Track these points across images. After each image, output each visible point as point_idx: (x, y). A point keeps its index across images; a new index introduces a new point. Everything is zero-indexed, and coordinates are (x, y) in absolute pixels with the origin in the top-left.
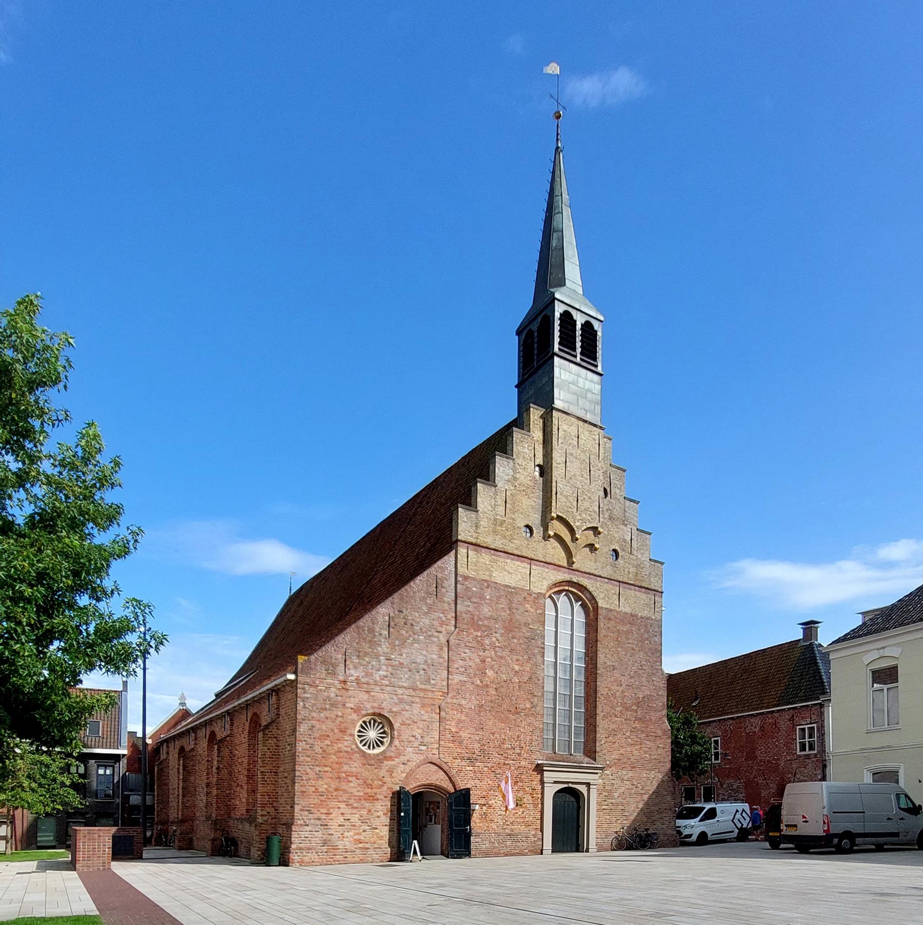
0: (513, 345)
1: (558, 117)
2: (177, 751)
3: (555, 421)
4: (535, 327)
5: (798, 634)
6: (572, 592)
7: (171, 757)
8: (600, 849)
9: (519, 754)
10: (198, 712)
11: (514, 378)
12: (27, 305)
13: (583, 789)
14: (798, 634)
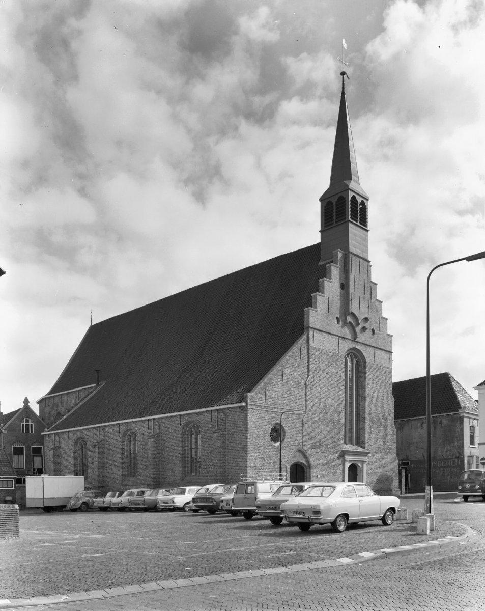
4: (334, 200)
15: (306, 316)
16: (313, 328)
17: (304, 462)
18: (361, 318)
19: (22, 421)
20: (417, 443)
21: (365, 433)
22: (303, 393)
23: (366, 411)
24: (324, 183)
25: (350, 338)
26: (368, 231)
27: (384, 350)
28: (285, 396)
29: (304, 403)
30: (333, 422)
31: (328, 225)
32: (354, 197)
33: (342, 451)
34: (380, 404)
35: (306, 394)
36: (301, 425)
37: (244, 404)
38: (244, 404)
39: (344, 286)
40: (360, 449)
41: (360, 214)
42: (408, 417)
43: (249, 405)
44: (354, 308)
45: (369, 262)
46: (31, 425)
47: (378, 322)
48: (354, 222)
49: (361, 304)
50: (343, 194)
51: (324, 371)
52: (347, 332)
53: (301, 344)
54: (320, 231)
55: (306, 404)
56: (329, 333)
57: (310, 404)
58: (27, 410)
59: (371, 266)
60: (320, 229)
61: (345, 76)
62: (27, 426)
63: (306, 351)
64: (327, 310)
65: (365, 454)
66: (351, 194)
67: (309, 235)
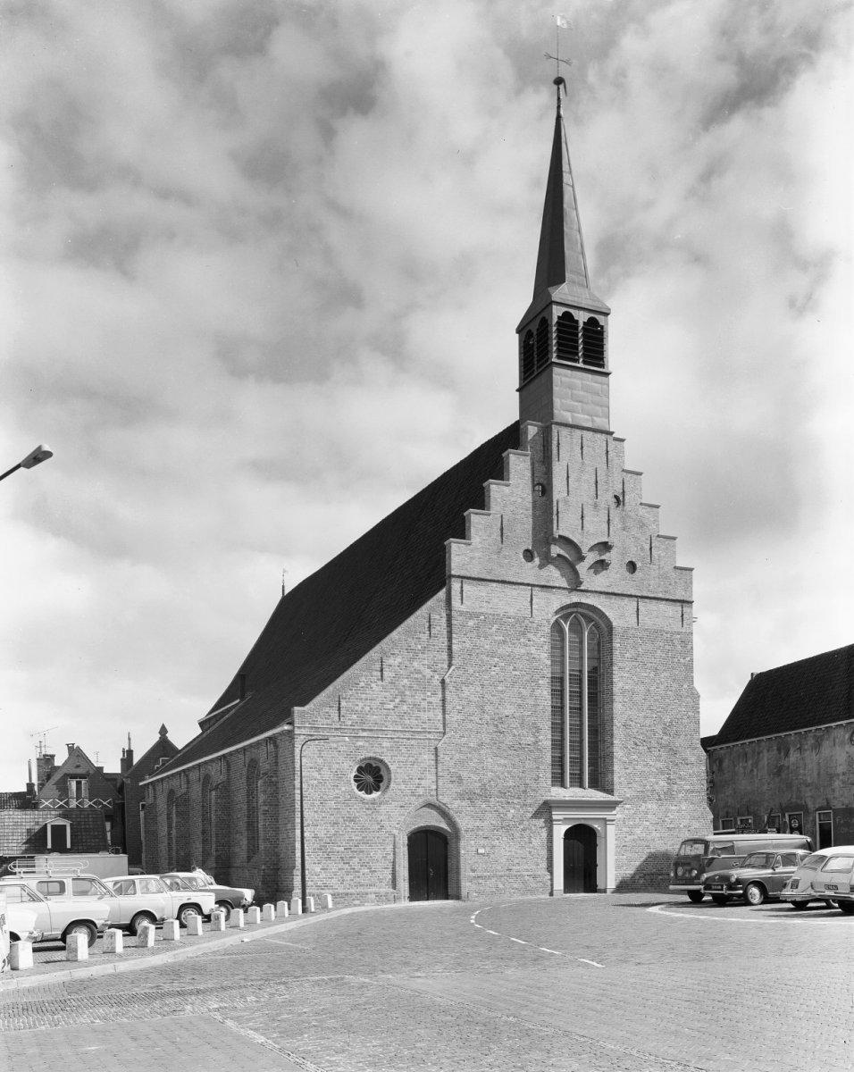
0: (514, 341)
2: (165, 794)
3: (555, 434)
4: (534, 327)
7: (158, 801)
10: (184, 748)
11: (515, 382)
15: (447, 555)
16: (459, 577)
17: (444, 825)
18: (585, 544)
20: (844, 774)
21: (612, 765)
22: (437, 699)
23: (615, 721)
24: (520, 301)
25: (565, 585)
26: (607, 374)
27: (667, 600)
28: (391, 707)
29: (440, 717)
30: (518, 747)
31: (529, 376)
32: (567, 317)
33: (546, 803)
35: (444, 700)
36: (433, 757)
39: (543, 487)
40: (598, 796)
42: (806, 727)
43: (299, 727)
44: (566, 525)
47: (648, 547)
48: (570, 363)
49: (586, 519)
50: (544, 314)
51: (492, 654)
52: (554, 575)
53: (432, 608)
54: (517, 390)
55: (444, 718)
56: (503, 582)
57: (453, 717)
60: (517, 386)
61: (561, 86)
63: (444, 620)
64: (499, 539)
65: (611, 806)
66: (557, 312)
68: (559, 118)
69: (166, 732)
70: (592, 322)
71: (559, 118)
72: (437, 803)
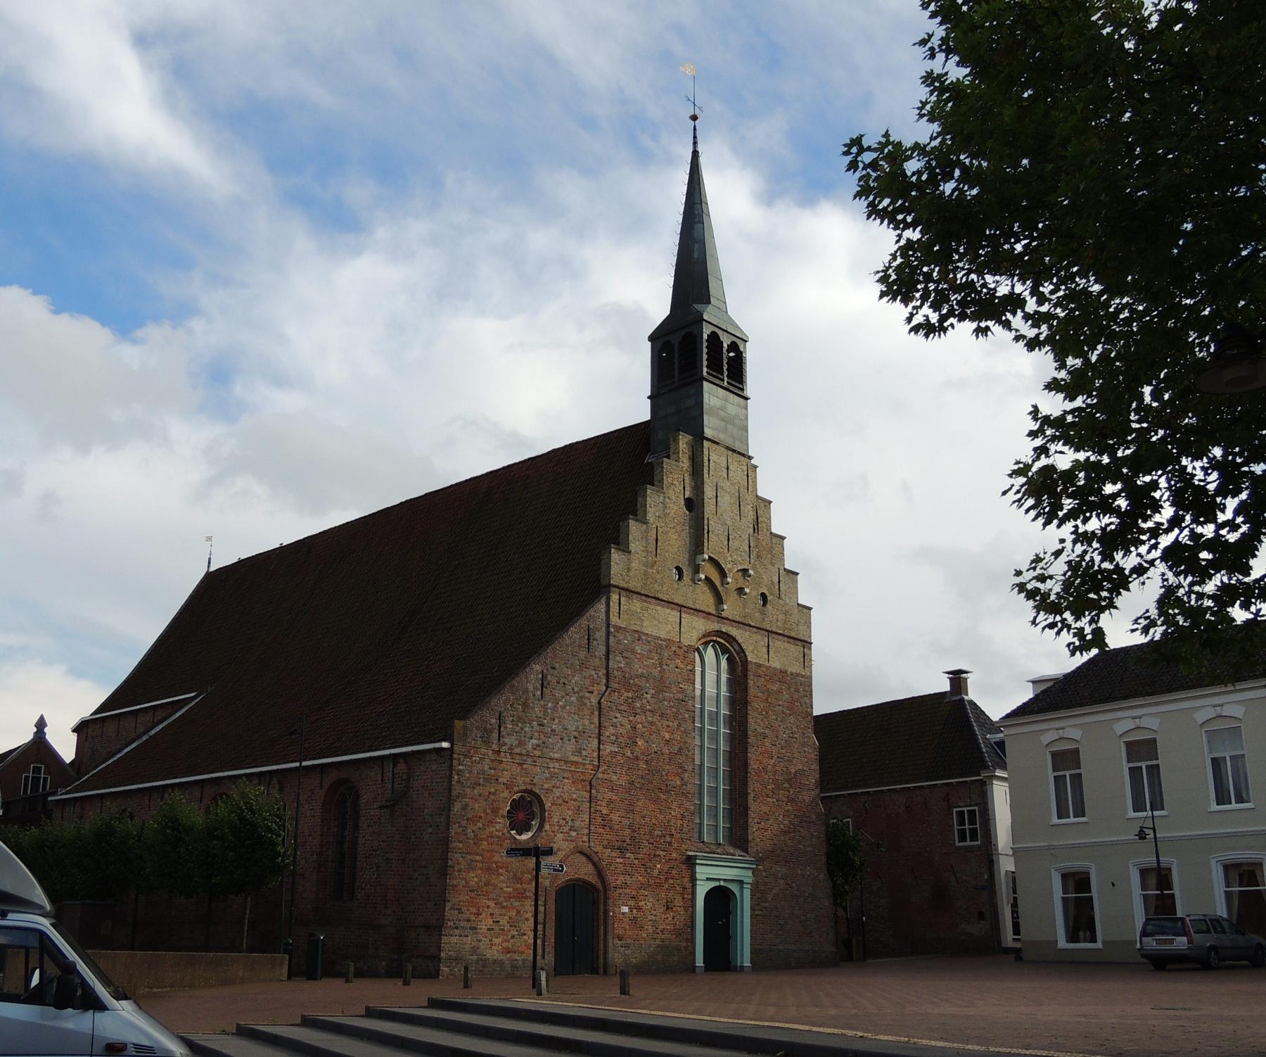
1: (694, 118)
4: (676, 340)
5: (944, 686)
6: (719, 643)
8: (766, 962)
9: (670, 843)
12: (957, 678)
13: (734, 888)
14: (944, 686)
19: (26, 770)
24: (658, 307)
26: (747, 399)
32: (714, 337)
34: (786, 757)
37: (445, 745)
38: (445, 745)
41: (731, 368)
45: (750, 458)
46: (45, 779)
58: (39, 746)
59: (756, 467)
62: (36, 780)
66: (707, 331)
67: (628, 403)
68: (695, 154)
69: (45, 725)
70: (734, 347)
71: (695, 154)
72: (588, 851)
